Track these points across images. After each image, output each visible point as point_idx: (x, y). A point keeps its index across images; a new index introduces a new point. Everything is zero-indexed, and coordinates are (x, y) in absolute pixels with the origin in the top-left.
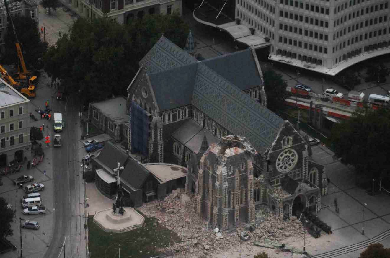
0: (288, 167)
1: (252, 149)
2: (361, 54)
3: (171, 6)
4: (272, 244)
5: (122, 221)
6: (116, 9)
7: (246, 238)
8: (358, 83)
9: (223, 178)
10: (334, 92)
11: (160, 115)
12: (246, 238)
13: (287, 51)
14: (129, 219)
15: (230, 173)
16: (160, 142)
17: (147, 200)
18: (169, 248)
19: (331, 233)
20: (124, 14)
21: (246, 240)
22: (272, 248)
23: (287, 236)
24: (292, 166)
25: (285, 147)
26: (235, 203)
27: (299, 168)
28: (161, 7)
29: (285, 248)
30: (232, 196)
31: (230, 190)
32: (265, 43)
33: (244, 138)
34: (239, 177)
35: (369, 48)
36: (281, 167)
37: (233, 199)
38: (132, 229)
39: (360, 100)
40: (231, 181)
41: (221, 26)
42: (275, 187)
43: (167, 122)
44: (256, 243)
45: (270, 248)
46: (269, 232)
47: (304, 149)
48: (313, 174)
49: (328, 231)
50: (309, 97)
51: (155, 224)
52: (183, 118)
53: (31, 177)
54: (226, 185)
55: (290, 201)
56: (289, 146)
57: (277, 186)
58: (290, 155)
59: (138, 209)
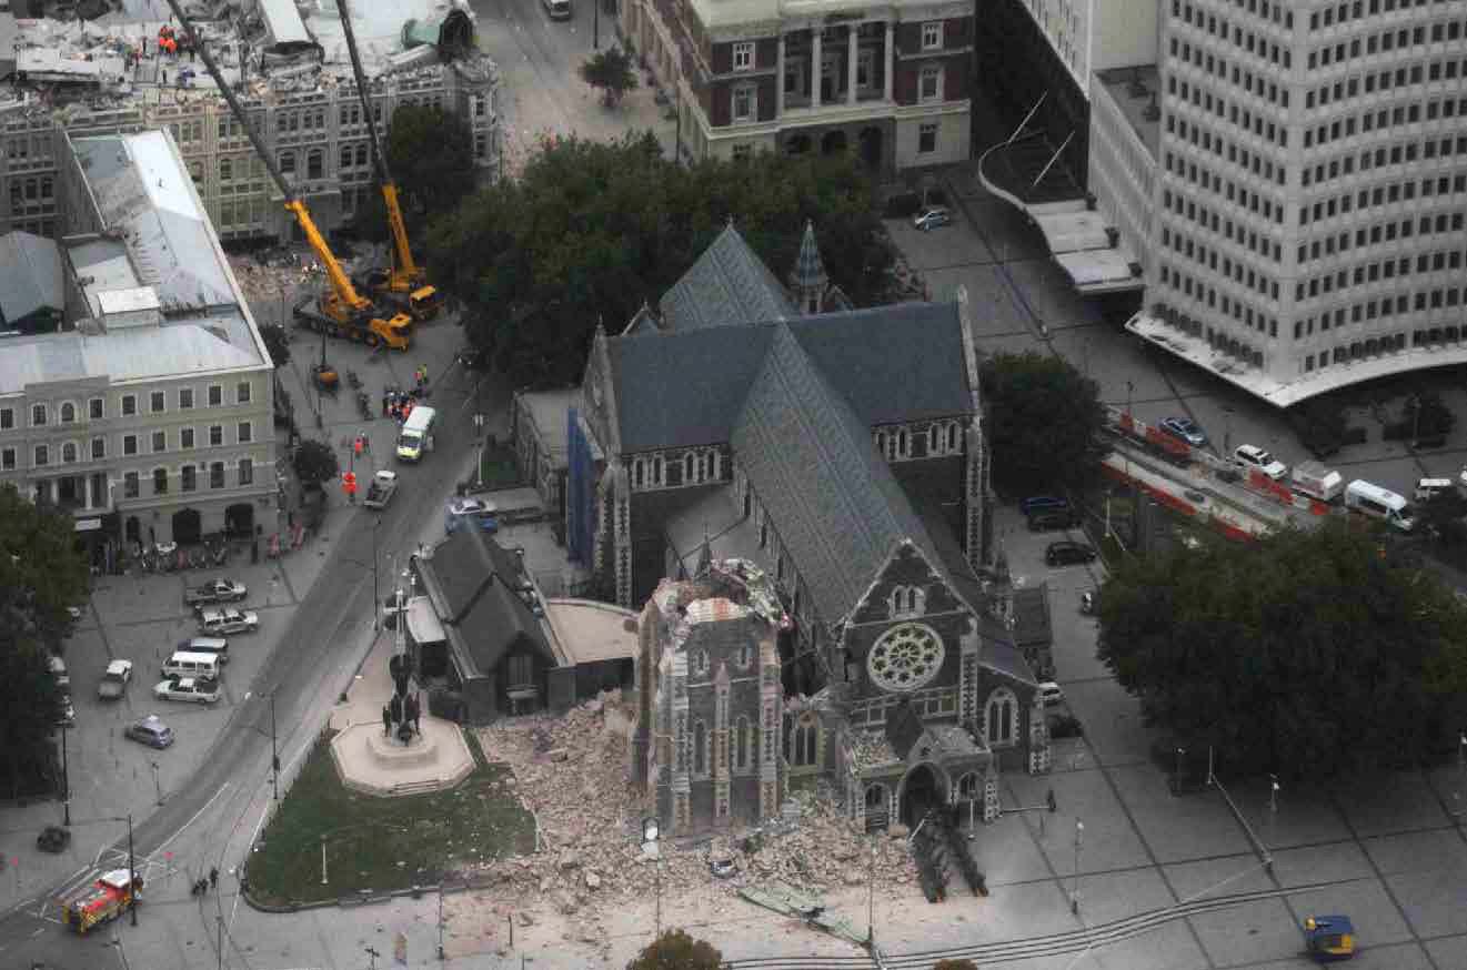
0: (912, 675)
1: (773, 610)
2: (1401, 352)
3: (934, 126)
4: (790, 903)
5: (402, 764)
6: (752, 120)
7: (723, 871)
8: (1359, 437)
9: (674, 684)
10: (1259, 457)
11: (626, 459)
12: (723, 871)
13: (1180, 313)
14: (430, 758)
15: (701, 673)
16: (623, 542)
17: (514, 710)
18: (493, 867)
19: (984, 893)
20: (776, 134)
21: (722, 877)
22: (784, 914)
23: (851, 884)
24: (928, 676)
25: (900, 617)
26: (719, 761)
27: (949, 683)
28: (901, 130)
29: (820, 920)
30: (709, 739)
31: (701, 718)
32: (1129, 279)
33: (760, 573)
34: (728, 689)
35: (1424, 338)
36: (889, 675)
37: (713, 750)
38: (420, 791)
39: (1322, 492)
40: (703, 700)
41: (1032, 209)
42: (865, 732)
43: (648, 485)
44: (744, 891)
45: (777, 911)
46: (796, 864)
47: (967, 629)
48: (1000, 709)
49: (977, 886)
50: (1184, 461)
51: (495, 785)
52: (701, 480)
53: (239, 589)
54: (682, 705)
55: (892, 781)
56: (913, 616)
57: (871, 729)
58: (920, 643)
59: (475, 731)
